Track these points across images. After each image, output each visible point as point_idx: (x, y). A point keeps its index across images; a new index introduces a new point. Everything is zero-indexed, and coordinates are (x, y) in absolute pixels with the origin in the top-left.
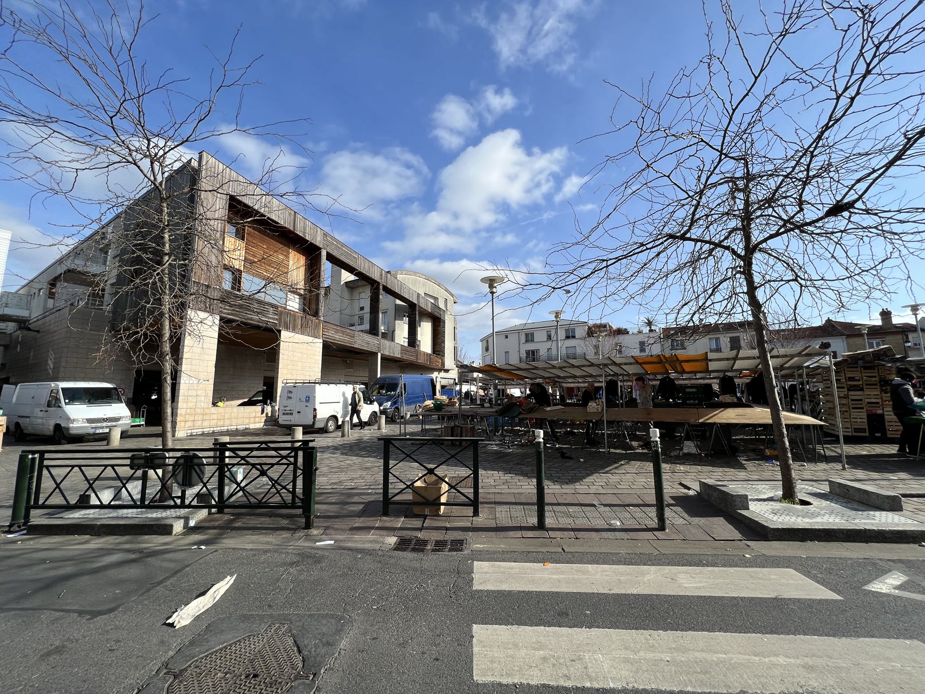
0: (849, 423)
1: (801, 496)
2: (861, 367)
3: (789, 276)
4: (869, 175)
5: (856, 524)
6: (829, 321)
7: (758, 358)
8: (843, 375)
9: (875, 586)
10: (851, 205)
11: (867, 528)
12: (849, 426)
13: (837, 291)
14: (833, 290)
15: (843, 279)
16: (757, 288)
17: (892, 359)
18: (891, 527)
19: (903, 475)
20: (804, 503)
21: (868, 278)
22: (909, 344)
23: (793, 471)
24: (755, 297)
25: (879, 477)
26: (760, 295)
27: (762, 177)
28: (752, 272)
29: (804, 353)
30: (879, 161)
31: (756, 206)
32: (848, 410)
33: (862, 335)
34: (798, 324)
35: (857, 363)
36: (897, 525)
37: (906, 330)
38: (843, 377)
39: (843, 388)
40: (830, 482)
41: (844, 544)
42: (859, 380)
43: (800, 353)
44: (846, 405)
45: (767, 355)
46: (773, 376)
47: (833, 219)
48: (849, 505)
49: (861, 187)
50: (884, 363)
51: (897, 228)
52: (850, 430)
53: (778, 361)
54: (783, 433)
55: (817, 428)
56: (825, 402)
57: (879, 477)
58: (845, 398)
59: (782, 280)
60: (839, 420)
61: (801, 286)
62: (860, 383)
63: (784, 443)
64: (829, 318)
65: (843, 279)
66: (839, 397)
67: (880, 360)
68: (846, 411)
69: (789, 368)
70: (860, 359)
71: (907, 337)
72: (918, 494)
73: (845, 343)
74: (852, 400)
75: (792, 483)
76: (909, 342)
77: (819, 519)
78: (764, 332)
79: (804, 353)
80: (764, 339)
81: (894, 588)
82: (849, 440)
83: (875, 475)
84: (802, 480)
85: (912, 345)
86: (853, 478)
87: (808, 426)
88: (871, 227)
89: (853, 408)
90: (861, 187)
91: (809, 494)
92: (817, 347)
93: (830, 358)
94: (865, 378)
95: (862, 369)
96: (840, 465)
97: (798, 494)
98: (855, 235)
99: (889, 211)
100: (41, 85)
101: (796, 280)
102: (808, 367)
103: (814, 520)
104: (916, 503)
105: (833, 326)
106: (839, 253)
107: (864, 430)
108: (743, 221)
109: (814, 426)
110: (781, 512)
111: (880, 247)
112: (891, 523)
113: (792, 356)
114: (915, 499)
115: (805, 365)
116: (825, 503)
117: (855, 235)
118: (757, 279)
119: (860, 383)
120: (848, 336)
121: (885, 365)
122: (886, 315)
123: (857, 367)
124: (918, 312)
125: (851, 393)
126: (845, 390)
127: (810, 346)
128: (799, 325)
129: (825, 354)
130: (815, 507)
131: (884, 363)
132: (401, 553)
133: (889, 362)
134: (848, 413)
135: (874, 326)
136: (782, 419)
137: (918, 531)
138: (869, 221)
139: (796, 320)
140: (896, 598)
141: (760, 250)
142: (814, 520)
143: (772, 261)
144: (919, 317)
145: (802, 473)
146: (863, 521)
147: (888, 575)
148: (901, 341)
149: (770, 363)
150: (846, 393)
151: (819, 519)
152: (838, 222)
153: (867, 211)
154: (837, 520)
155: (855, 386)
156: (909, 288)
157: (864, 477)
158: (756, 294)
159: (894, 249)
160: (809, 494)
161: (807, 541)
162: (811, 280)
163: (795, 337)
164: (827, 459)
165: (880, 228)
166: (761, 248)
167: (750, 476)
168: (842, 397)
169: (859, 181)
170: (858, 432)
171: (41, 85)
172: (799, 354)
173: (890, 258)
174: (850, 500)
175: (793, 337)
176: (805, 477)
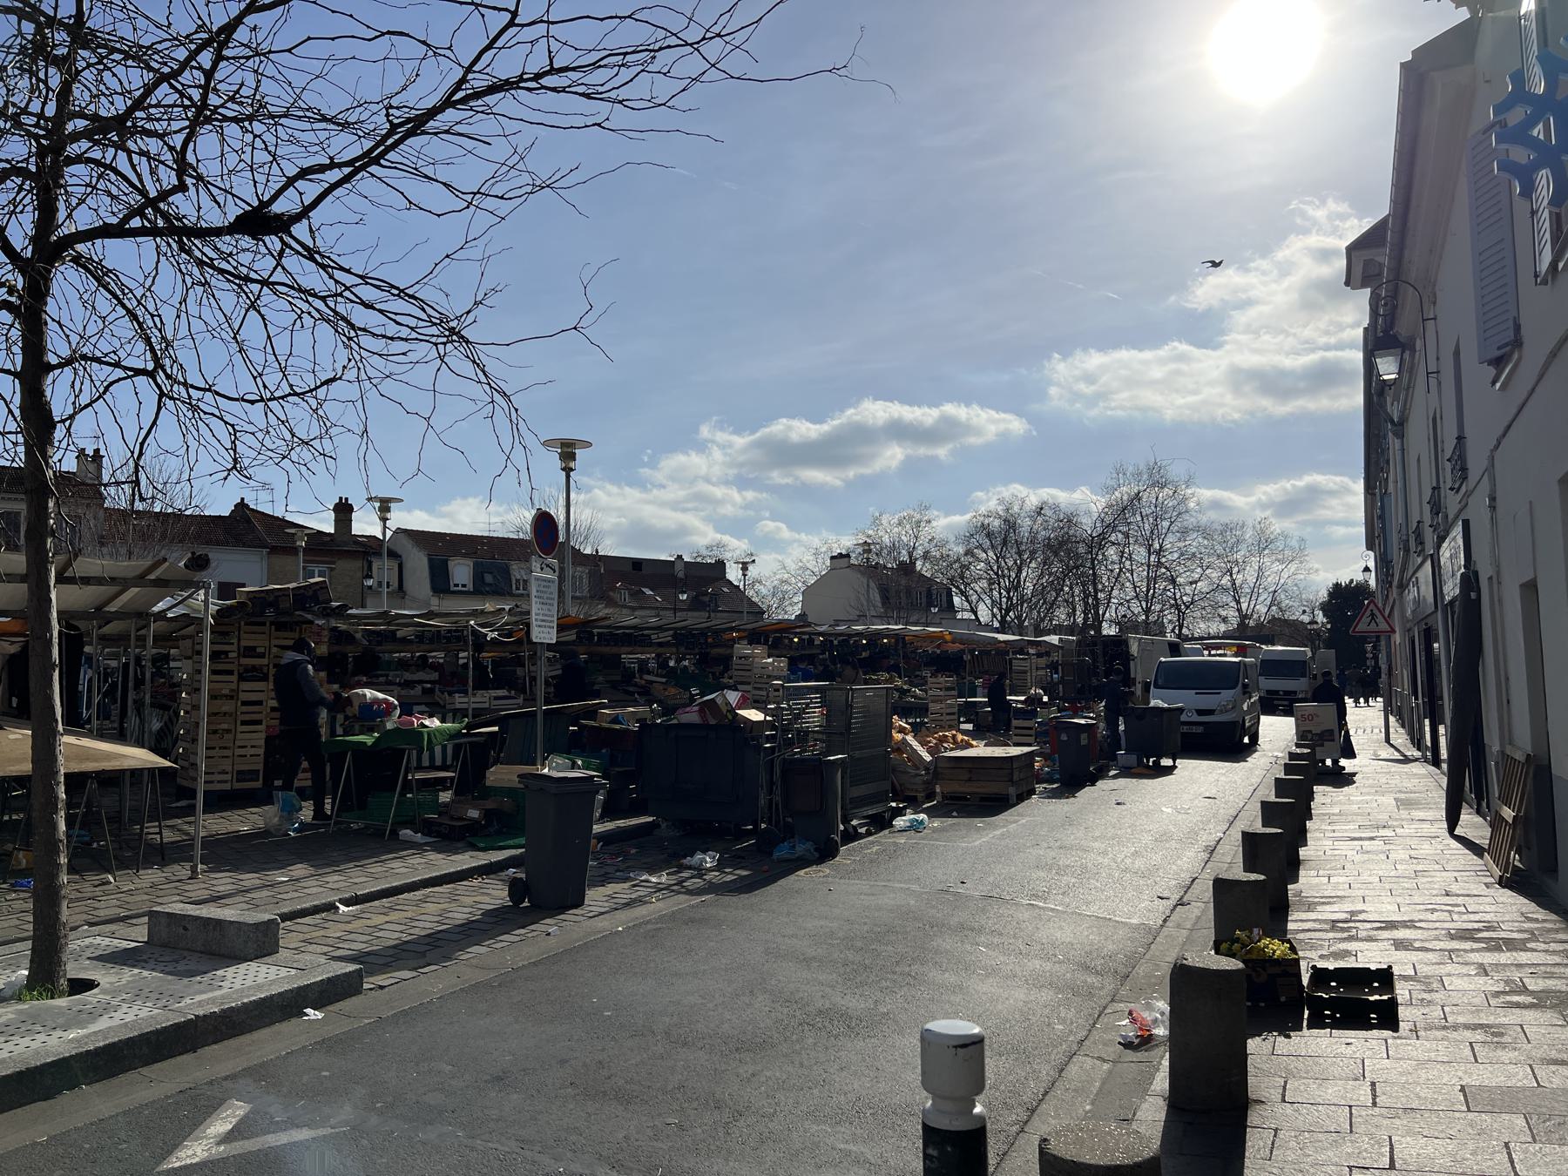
0: (229, 761)
1: (74, 969)
2: (272, 623)
3: (139, 358)
4: (322, 169)
5: (179, 1011)
6: (241, 506)
7: (23, 579)
8: (235, 641)
9: (182, 1154)
10: (282, 225)
11: (201, 1012)
12: (229, 769)
13: (233, 426)
14: (226, 423)
15: (252, 402)
16: (53, 368)
17: (324, 608)
18: (247, 996)
19: (299, 870)
20: (81, 986)
21: (297, 412)
22: (370, 582)
23: (65, 904)
24: (42, 394)
25: (258, 882)
26: (59, 392)
27: (113, 50)
28: (44, 316)
29: (152, 577)
30: (348, 147)
31: (81, 124)
32: (233, 727)
33: (293, 551)
34: (140, 494)
35: (262, 614)
36: (259, 987)
37: (369, 548)
38: (235, 647)
39: (230, 673)
40: (152, 915)
41: (145, 1071)
42: (262, 656)
43: (142, 576)
44: (231, 715)
45: (47, 571)
46: (56, 634)
47: (246, 241)
48: (181, 967)
49: (310, 189)
50: (309, 617)
51: (360, 316)
52: (228, 777)
53: (80, 597)
54: (56, 798)
55: (154, 775)
56: (189, 708)
57: (258, 882)
58: (232, 697)
59: (117, 365)
60: (202, 751)
61: (162, 395)
62: (265, 661)
63: (54, 826)
64: (243, 499)
65: (252, 402)
66: (213, 697)
67: (304, 609)
68: (228, 731)
69: (120, 615)
70: (271, 605)
71: (370, 568)
72: (315, 906)
73: (265, 564)
74: (244, 703)
75: (59, 938)
76: (371, 577)
77: (103, 1024)
78: (51, 504)
79: (152, 577)
80: (46, 524)
81: (219, 1144)
82: (220, 801)
83: (250, 879)
84: (91, 924)
85: (376, 585)
86: (205, 894)
87: (136, 774)
88: (315, 295)
89: (244, 723)
90: (310, 189)
91: (100, 958)
92: (182, 564)
93: (206, 595)
94: (275, 650)
95: (273, 627)
96: (188, 865)
97: (69, 967)
98: (290, 303)
99: (348, 271)
100: (457, 193)
101: (151, 374)
102: (161, 615)
103: (93, 1028)
104: (306, 929)
105: (249, 521)
106: (253, 331)
107: (252, 775)
108: (41, 153)
109: (151, 771)
110: (11, 1030)
111: (326, 345)
112: (242, 990)
113: (123, 583)
114: (307, 920)
115: (156, 609)
116: (129, 974)
117: (290, 303)
118: (57, 346)
119: (265, 661)
120: (274, 550)
121: (311, 622)
122: (343, 510)
123: (263, 624)
124: (388, 515)
125: (245, 686)
126: (234, 678)
127: (165, 560)
128: (142, 499)
129: (198, 586)
130: (104, 992)
131: (309, 617)
132: (554, 932)
133: (319, 617)
134: (231, 736)
135: (320, 532)
136: (60, 759)
137: (291, 991)
138: (312, 277)
139: (137, 483)
140: (224, 1160)
141: (77, 260)
142: (93, 1028)
143: (103, 303)
144: (393, 524)
145: (97, 905)
146: (198, 998)
147: (214, 1116)
148: (359, 574)
149: (53, 596)
150: (234, 686)
151: (103, 1024)
152: (254, 256)
153: (311, 254)
154: (144, 1013)
155: (254, 668)
156: (361, 455)
157: (229, 887)
158: (48, 393)
159: (350, 360)
160: (100, 958)
161: (60, 1092)
162: (185, 384)
163: (164, 536)
164: (162, 855)
165: (332, 305)
166: (80, 256)
167: (267, 878)
168: (226, 696)
169: (304, 173)
170: (245, 780)
171: (457, 193)
172: (140, 580)
173: (340, 378)
174: (185, 953)
175: (157, 536)
176: (101, 913)
